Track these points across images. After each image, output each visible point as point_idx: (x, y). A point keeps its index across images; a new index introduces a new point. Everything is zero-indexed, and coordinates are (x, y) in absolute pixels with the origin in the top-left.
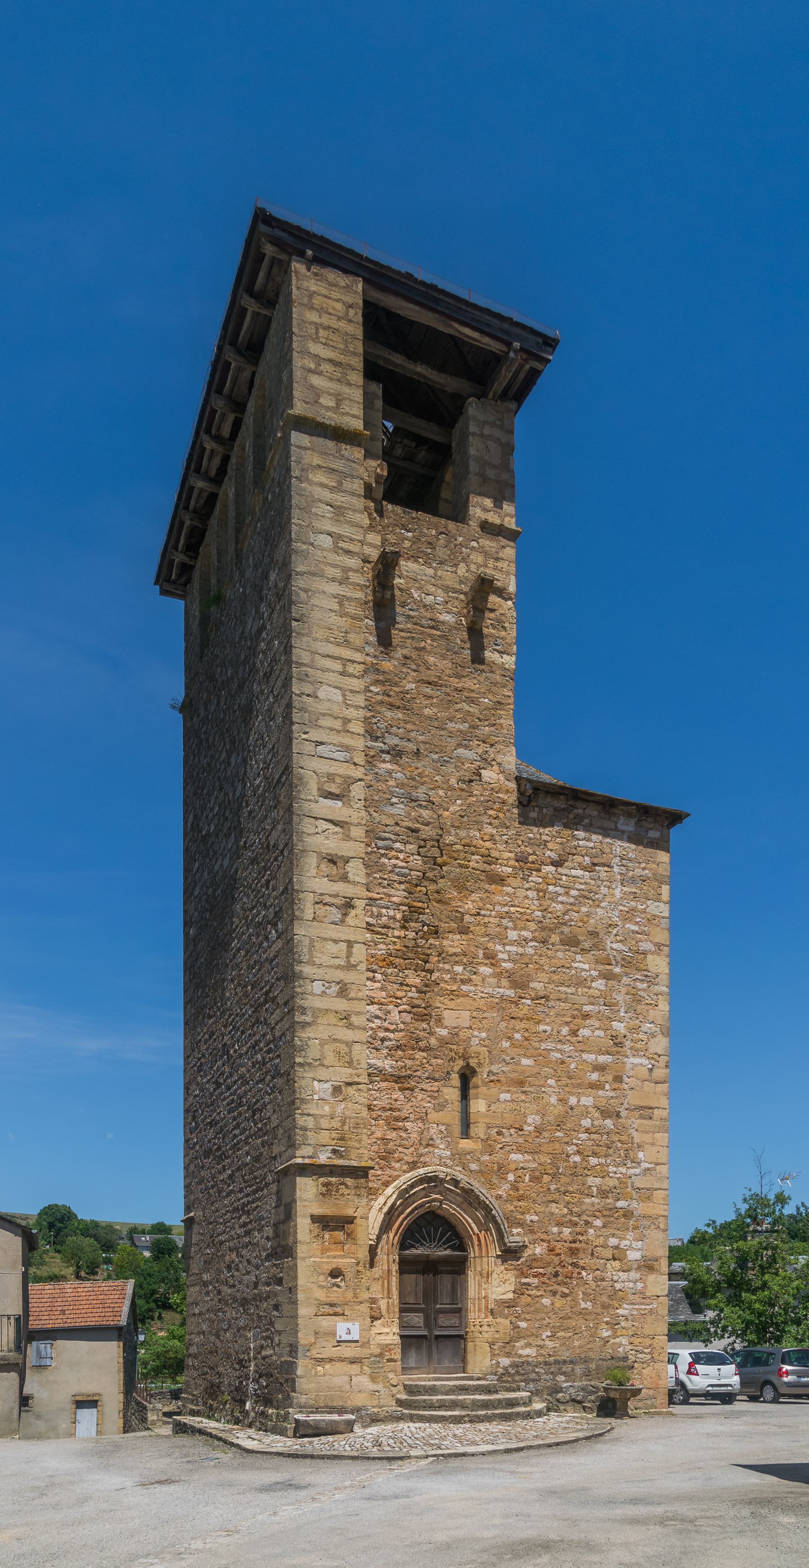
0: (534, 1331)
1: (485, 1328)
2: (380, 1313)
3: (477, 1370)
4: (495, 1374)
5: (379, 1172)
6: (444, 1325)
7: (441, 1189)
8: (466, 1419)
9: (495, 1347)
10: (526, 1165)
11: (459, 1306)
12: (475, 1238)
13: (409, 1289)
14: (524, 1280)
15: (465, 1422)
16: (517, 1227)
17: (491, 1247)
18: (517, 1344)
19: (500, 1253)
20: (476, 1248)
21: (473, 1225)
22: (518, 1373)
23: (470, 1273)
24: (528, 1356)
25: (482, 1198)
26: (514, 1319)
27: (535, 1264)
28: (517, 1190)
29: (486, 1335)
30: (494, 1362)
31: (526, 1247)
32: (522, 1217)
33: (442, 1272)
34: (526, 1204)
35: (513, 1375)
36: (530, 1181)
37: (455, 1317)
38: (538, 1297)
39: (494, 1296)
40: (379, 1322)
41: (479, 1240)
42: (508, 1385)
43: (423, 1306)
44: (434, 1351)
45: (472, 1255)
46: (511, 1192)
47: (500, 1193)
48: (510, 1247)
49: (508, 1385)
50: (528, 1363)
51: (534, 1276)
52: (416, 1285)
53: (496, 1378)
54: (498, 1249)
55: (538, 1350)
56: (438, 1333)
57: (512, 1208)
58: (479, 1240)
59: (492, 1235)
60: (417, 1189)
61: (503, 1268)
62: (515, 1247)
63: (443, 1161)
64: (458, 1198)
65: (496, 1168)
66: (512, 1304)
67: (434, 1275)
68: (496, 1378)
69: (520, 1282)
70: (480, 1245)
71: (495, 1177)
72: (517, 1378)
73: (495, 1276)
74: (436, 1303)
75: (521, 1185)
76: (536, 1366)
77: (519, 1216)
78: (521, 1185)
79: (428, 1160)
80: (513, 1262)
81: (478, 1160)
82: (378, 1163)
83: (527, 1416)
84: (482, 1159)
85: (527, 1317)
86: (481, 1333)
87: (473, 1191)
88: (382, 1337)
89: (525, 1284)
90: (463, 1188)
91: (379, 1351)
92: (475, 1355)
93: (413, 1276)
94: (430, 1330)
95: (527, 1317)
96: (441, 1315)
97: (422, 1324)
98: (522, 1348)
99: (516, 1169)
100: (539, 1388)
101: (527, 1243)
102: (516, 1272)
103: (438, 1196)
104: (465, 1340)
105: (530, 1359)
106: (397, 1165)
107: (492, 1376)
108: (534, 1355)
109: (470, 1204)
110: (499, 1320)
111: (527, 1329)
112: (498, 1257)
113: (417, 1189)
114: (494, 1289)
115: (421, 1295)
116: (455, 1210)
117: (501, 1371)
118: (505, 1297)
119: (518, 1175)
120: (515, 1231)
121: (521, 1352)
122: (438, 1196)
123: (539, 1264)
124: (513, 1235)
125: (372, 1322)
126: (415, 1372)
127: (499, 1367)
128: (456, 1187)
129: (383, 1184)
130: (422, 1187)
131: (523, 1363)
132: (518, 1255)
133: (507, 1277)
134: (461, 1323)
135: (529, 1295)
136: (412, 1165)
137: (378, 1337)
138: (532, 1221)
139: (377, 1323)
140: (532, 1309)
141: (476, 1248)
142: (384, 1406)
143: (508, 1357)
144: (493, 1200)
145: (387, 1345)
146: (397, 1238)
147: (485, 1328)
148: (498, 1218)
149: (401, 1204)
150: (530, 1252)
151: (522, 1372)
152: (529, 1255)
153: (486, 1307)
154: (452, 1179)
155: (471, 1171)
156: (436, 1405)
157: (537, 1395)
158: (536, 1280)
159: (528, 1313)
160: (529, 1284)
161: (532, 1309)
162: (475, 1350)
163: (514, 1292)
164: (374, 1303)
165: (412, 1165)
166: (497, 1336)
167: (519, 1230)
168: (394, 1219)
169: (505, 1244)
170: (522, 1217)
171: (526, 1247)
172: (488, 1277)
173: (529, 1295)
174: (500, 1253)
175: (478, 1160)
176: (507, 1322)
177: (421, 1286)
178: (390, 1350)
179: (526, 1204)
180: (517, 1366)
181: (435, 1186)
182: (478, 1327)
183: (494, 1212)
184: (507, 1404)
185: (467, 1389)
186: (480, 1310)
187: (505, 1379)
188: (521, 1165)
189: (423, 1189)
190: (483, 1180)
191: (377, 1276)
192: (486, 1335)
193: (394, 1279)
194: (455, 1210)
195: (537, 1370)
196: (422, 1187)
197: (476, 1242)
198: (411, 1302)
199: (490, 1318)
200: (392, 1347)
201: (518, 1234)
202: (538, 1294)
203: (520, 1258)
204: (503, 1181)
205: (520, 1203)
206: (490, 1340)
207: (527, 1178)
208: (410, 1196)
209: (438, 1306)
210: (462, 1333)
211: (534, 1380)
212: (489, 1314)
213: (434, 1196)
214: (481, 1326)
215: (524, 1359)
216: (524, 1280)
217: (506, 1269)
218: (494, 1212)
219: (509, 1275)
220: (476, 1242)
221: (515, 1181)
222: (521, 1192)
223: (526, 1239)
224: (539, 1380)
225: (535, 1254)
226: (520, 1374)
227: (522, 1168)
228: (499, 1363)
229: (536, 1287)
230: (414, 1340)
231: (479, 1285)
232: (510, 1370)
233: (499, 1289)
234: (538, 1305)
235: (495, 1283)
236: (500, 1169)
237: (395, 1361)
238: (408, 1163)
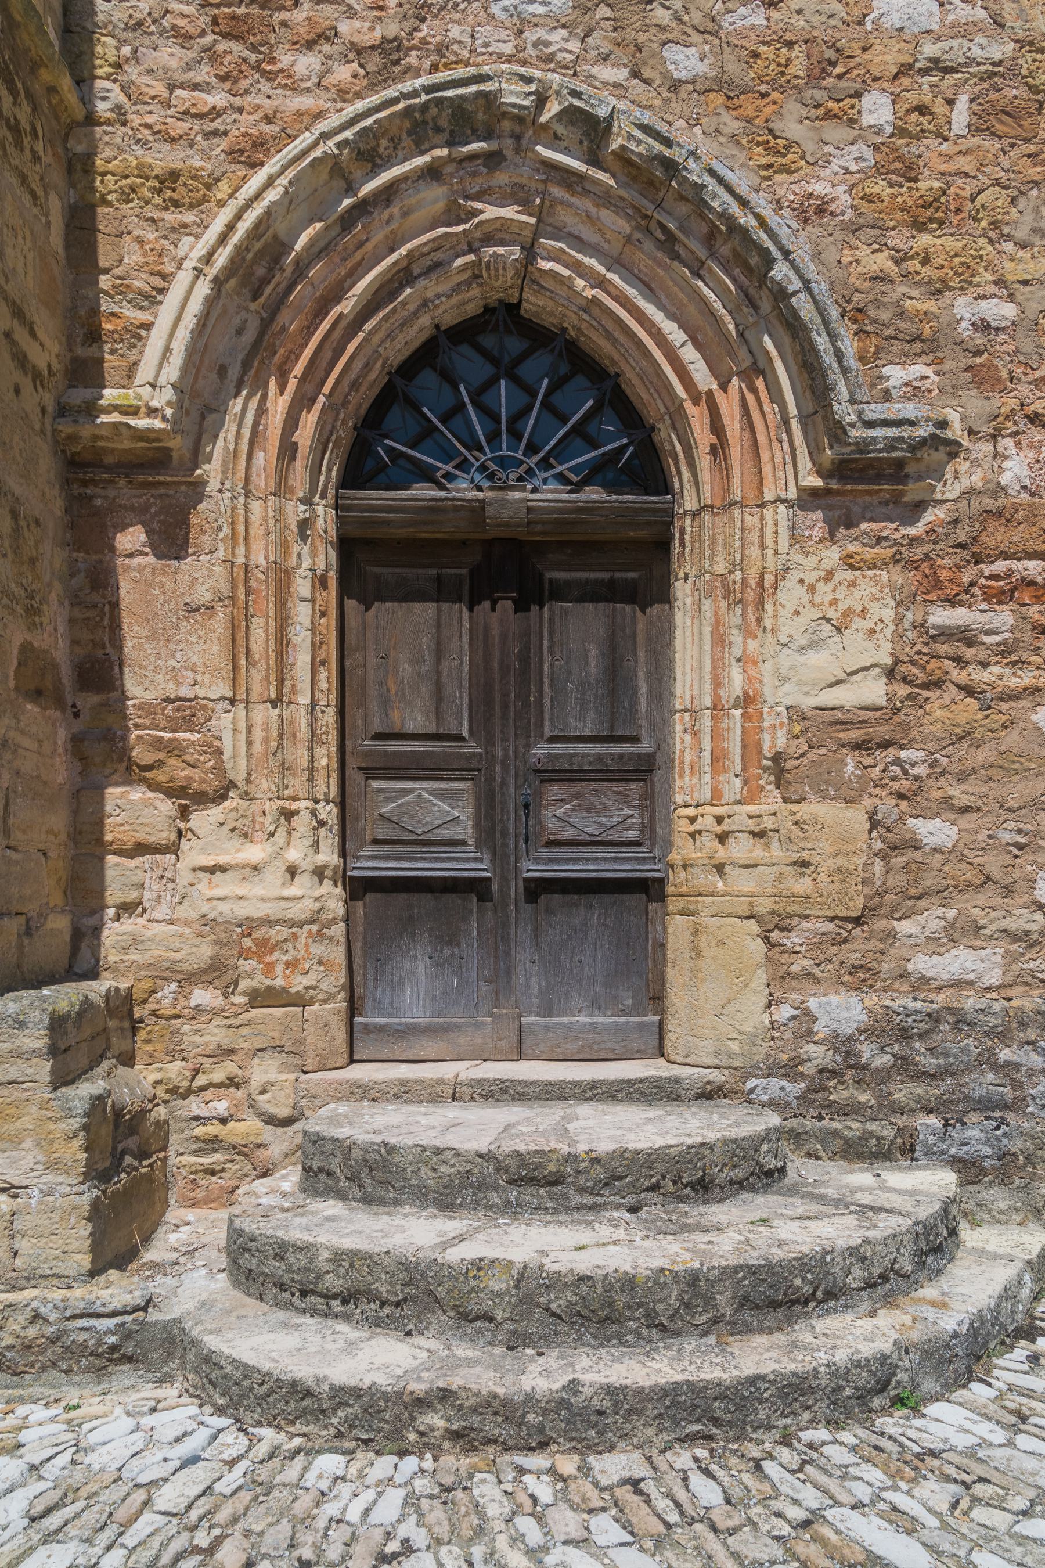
0: (994, 862)
1: (740, 848)
2: (219, 769)
3: (704, 1053)
4: (791, 1070)
5: (217, 99)
6: (568, 833)
7: (525, 175)
8: (435, 1421)
9: (792, 940)
10: (956, 50)
11: (645, 746)
12: (697, 417)
13: (406, 669)
14: (942, 616)
15: (426, 1444)
16: (904, 359)
17: (774, 454)
18: (904, 927)
19: (815, 482)
20: (704, 462)
21: (689, 354)
22: (905, 1067)
23: (682, 590)
24: (958, 984)
25: (720, 200)
26: (887, 807)
27: (997, 537)
28: (910, 173)
29: (744, 882)
30: (785, 1012)
31: (953, 450)
32: (930, 305)
33: (559, 593)
34: (953, 244)
35: (883, 1077)
36: (974, 130)
37: (625, 799)
38: (1013, 696)
39: (790, 695)
40: (215, 813)
41: (717, 428)
42: (854, 1127)
43: (472, 748)
44: (524, 955)
45: (690, 503)
46: (879, 187)
47: (819, 188)
48: (863, 446)
49: (854, 1127)
50: (961, 1021)
51: (998, 597)
52: (439, 654)
53: (795, 1089)
54: (805, 462)
55: (1012, 958)
56: (533, 869)
57: (882, 262)
58: (717, 428)
59: (776, 395)
60: (396, 171)
61: (832, 555)
62: (892, 444)
63: (530, 36)
64: (607, 216)
65: (798, 68)
66: (883, 731)
67: (522, 606)
68: (795, 1089)
69: (920, 626)
70: (719, 450)
71: (793, 108)
72: (902, 1092)
73: (791, 593)
74: (530, 732)
75: (931, 151)
76: (1003, 1036)
77: (919, 303)
78: (931, 151)
79: (455, 32)
80: (886, 528)
81: (710, 29)
82: (211, 55)
83: (863, 1397)
84: (727, 22)
85: (957, 792)
86: (720, 869)
87: (670, 166)
88: (225, 886)
89: (945, 634)
90: (623, 156)
91: (204, 952)
92: (695, 974)
93: (425, 611)
94: (500, 857)
95: (957, 792)
96: (556, 791)
97: (465, 829)
98: (933, 944)
99: (905, 70)
100: (1016, 1145)
101: (956, 431)
102: (897, 576)
103: (510, 212)
104: (661, 897)
105: (970, 1002)
106: (306, 64)
107: (775, 1083)
108: (994, 978)
109: (669, 243)
110: (813, 808)
111: (955, 853)
112: (809, 499)
113: (396, 171)
114: (787, 659)
115: (459, 695)
116: (601, 283)
117: (818, 1055)
118: (845, 696)
119: (912, 98)
120: (896, 375)
121: (923, 964)
122: (510, 212)
123: (1018, 534)
124: (887, 396)
125: (184, 813)
126: (429, 1047)
127: (808, 1035)
128: (594, 161)
129: (233, 154)
130: (420, 161)
131: (935, 1018)
132: (913, 491)
133: (852, 600)
134: (649, 827)
135: (969, 690)
136: (375, 62)
137: (206, 887)
138: (983, 326)
139: (203, 819)
140: (982, 756)
141: (704, 462)
142: (32, 1278)
143: (860, 988)
144: (783, 224)
145: (248, 926)
146: (309, 421)
147: (740, 848)
148: (802, 304)
149: (319, 250)
150: (977, 479)
151: (930, 1063)
152: (970, 493)
153: (750, 747)
154: (570, 115)
155: (675, 86)
156: (332, 1282)
157: (1004, 1180)
158: (1004, 617)
159: (962, 777)
160: (966, 636)
161: (982, 756)
162: (697, 952)
163: (890, 673)
164: (188, 723)
165: (375, 62)
166: (803, 885)
167: (919, 369)
168: (291, 321)
169: (837, 431)
170: (930, 305)
171: (953, 450)
172: (760, 604)
173: (969, 690)
174: (815, 482)
175: (710, 29)
176: (856, 818)
177: (461, 646)
178: (265, 947)
179: (953, 244)
180: (905, 1035)
181: (493, 160)
182: (708, 842)
183: (780, 271)
184: (744, 1301)
185: (555, 1181)
186: (718, 760)
187: (840, 1094)
188: (930, 50)
189: (432, 173)
190: (733, 126)
191: (203, 594)
192: (744, 882)
193: (302, 614)
194: (601, 283)
195: (1005, 1054)
196: (420, 161)
197: (702, 437)
198: (411, 727)
199: (772, 799)
200: (277, 933)
201: (914, 391)
202: (1014, 682)
203: (919, 507)
204: (835, 132)
205: (925, 240)
206: (764, 906)
207: (960, 117)
208: (363, 207)
209: (542, 749)
210: (647, 870)
211: (986, 1105)
212: (766, 780)
213: (491, 212)
214: (722, 838)
215: (940, 999)
216: (942, 616)
217: (849, 562)
218: (780, 271)
219: (866, 588)
220: (702, 437)
221: (900, 132)
222: (929, 184)
223: (953, 416)
224: (1017, 1105)
225: (1001, 490)
226: (919, 1075)
227: (936, 65)
228: (809, 1016)
229: (1004, 651)
230: (426, 901)
231: (720, 640)
232: (866, 1051)
233: (814, 658)
234: (1011, 739)
235: (790, 628)
236: (820, 70)
237: (301, 1001)
238: (359, 51)
